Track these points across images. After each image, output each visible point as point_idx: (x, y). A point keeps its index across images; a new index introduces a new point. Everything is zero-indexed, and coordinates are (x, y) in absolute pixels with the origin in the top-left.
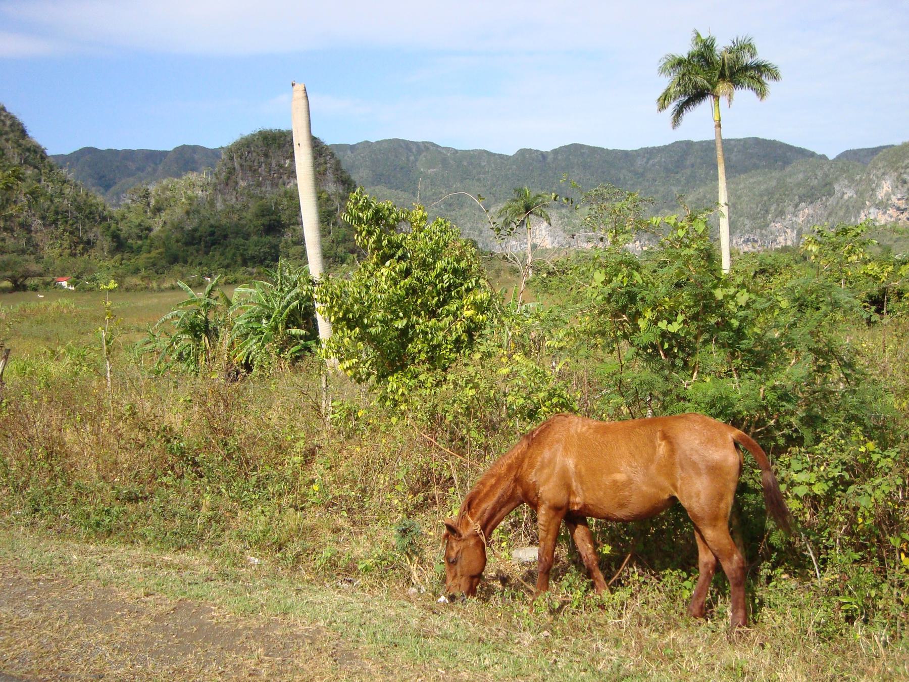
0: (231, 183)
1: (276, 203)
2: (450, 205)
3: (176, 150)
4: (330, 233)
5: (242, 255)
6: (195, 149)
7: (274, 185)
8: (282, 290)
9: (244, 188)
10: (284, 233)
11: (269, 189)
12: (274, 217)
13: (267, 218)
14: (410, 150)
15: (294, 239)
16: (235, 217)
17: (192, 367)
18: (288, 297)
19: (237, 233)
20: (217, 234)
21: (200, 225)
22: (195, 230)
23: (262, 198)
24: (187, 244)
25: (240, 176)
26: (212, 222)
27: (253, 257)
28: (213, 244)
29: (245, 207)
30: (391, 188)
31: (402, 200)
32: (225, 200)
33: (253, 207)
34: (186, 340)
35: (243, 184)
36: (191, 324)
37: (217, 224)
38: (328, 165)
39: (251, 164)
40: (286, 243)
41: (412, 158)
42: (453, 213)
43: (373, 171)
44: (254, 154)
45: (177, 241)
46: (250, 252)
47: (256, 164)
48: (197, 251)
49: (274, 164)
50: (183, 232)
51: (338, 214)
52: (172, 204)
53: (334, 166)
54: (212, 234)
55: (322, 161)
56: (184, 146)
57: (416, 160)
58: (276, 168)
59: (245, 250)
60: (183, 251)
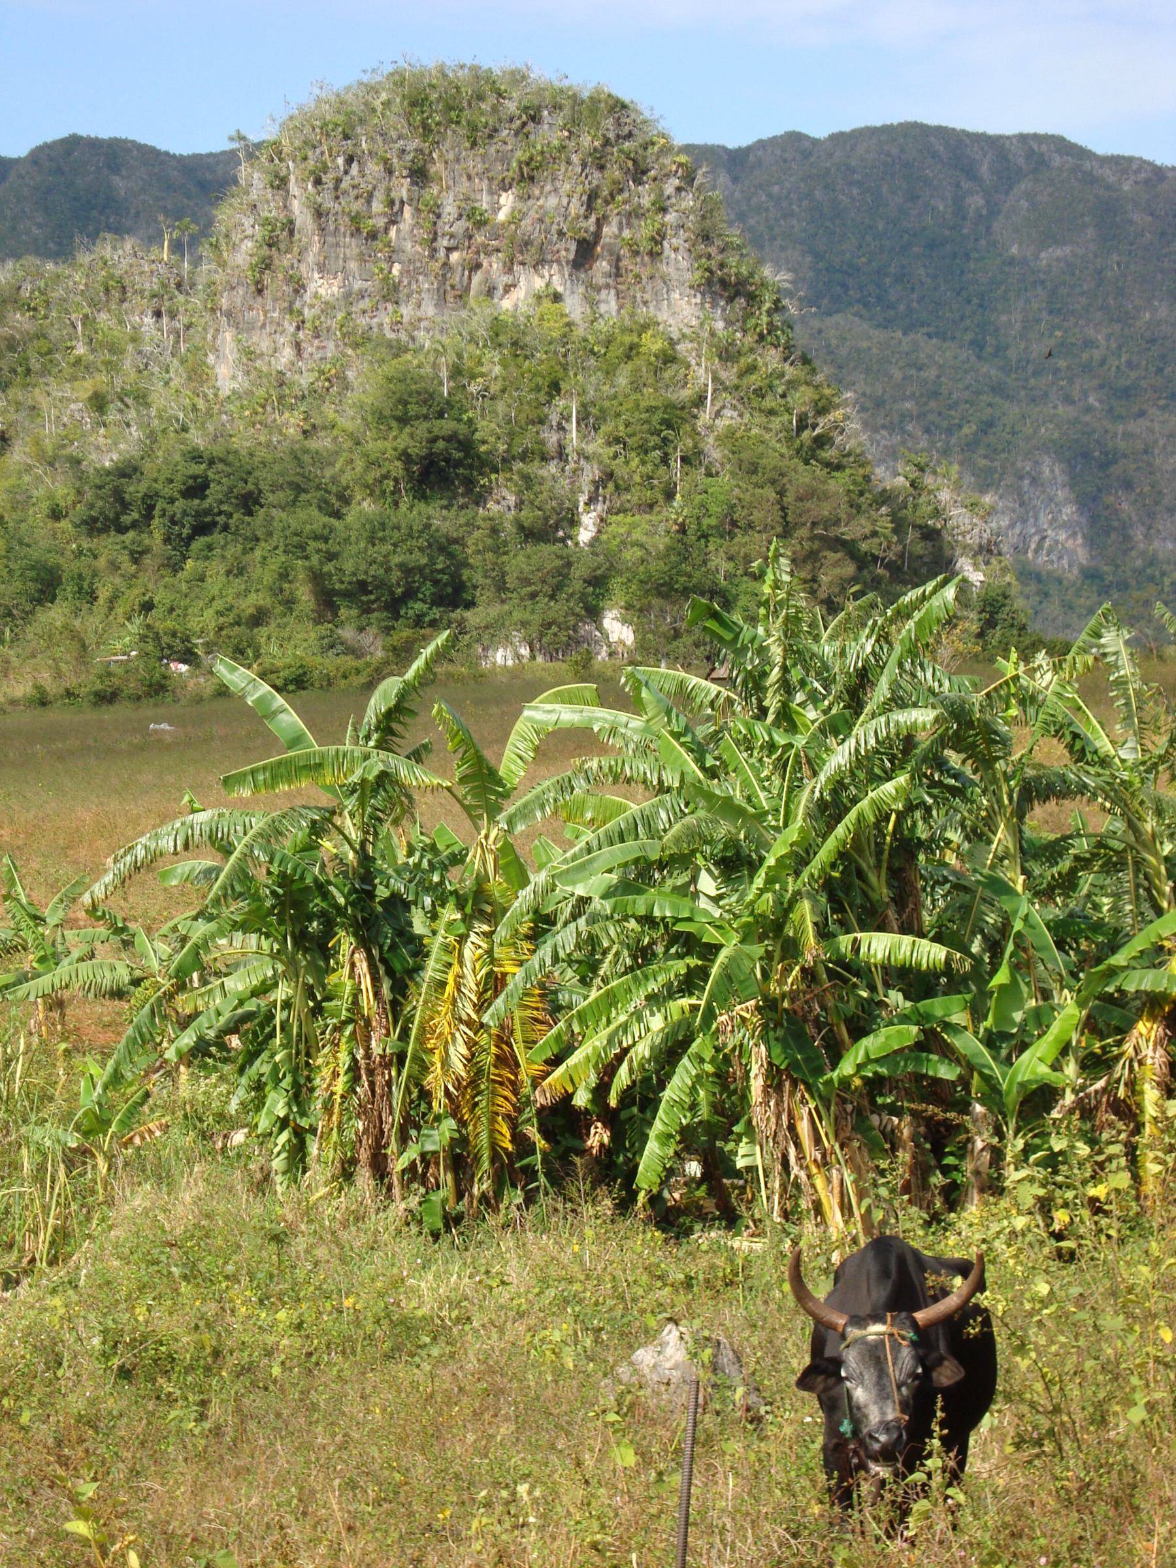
0: (275, 283)
1: (456, 372)
2: (1126, 393)
3: (41, 155)
4: (670, 495)
5: (317, 578)
6: (115, 154)
7: (452, 293)
8: (787, 719)
9: (328, 308)
10: (489, 490)
11: (429, 310)
12: (446, 426)
13: (422, 429)
14: (970, 173)
15: (528, 516)
16: (292, 423)
17: (278, 1104)
18: (839, 757)
19: (298, 489)
20: (215, 492)
21: (149, 453)
22: (127, 471)
23: (398, 350)
24: (93, 526)
25: (311, 257)
26: (197, 439)
27: (362, 586)
28: (202, 529)
29: (335, 381)
30: (885, 325)
31: (931, 374)
32: (250, 354)
33: (366, 382)
34: (249, 965)
35: (323, 287)
36: (284, 880)
37: (218, 450)
38: (671, 218)
39: (357, 206)
40: (495, 531)
41: (976, 201)
42: (1137, 426)
43: (818, 256)
44: (374, 168)
45: (56, 514)
46: (349, 566)
47: (377, 206)
48: (137, 557)
49: (450, 209)
50: (81, 477)
51: (705, 417)
52: (35, 364)
53: (692, 221)
54: (196, 489)
55: (646, 201)
56: (73, 142)
57: (993, 210)
58: (460, 226)
59: (331, 557)
60: (80, 553)
